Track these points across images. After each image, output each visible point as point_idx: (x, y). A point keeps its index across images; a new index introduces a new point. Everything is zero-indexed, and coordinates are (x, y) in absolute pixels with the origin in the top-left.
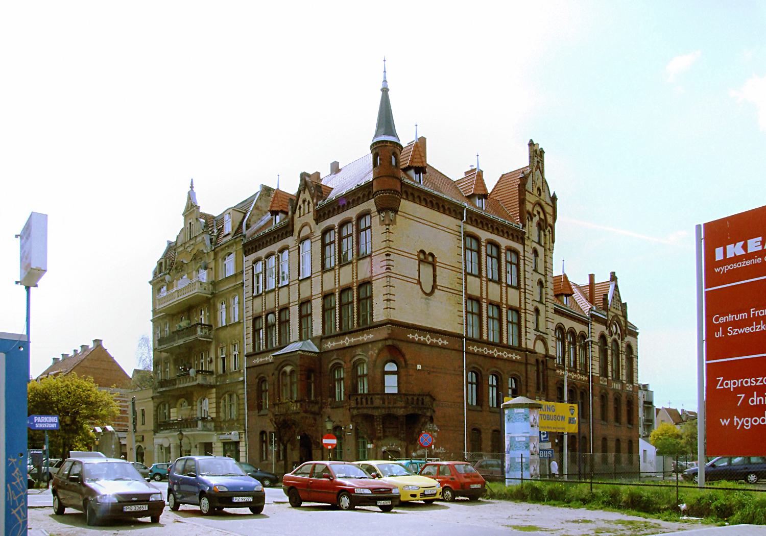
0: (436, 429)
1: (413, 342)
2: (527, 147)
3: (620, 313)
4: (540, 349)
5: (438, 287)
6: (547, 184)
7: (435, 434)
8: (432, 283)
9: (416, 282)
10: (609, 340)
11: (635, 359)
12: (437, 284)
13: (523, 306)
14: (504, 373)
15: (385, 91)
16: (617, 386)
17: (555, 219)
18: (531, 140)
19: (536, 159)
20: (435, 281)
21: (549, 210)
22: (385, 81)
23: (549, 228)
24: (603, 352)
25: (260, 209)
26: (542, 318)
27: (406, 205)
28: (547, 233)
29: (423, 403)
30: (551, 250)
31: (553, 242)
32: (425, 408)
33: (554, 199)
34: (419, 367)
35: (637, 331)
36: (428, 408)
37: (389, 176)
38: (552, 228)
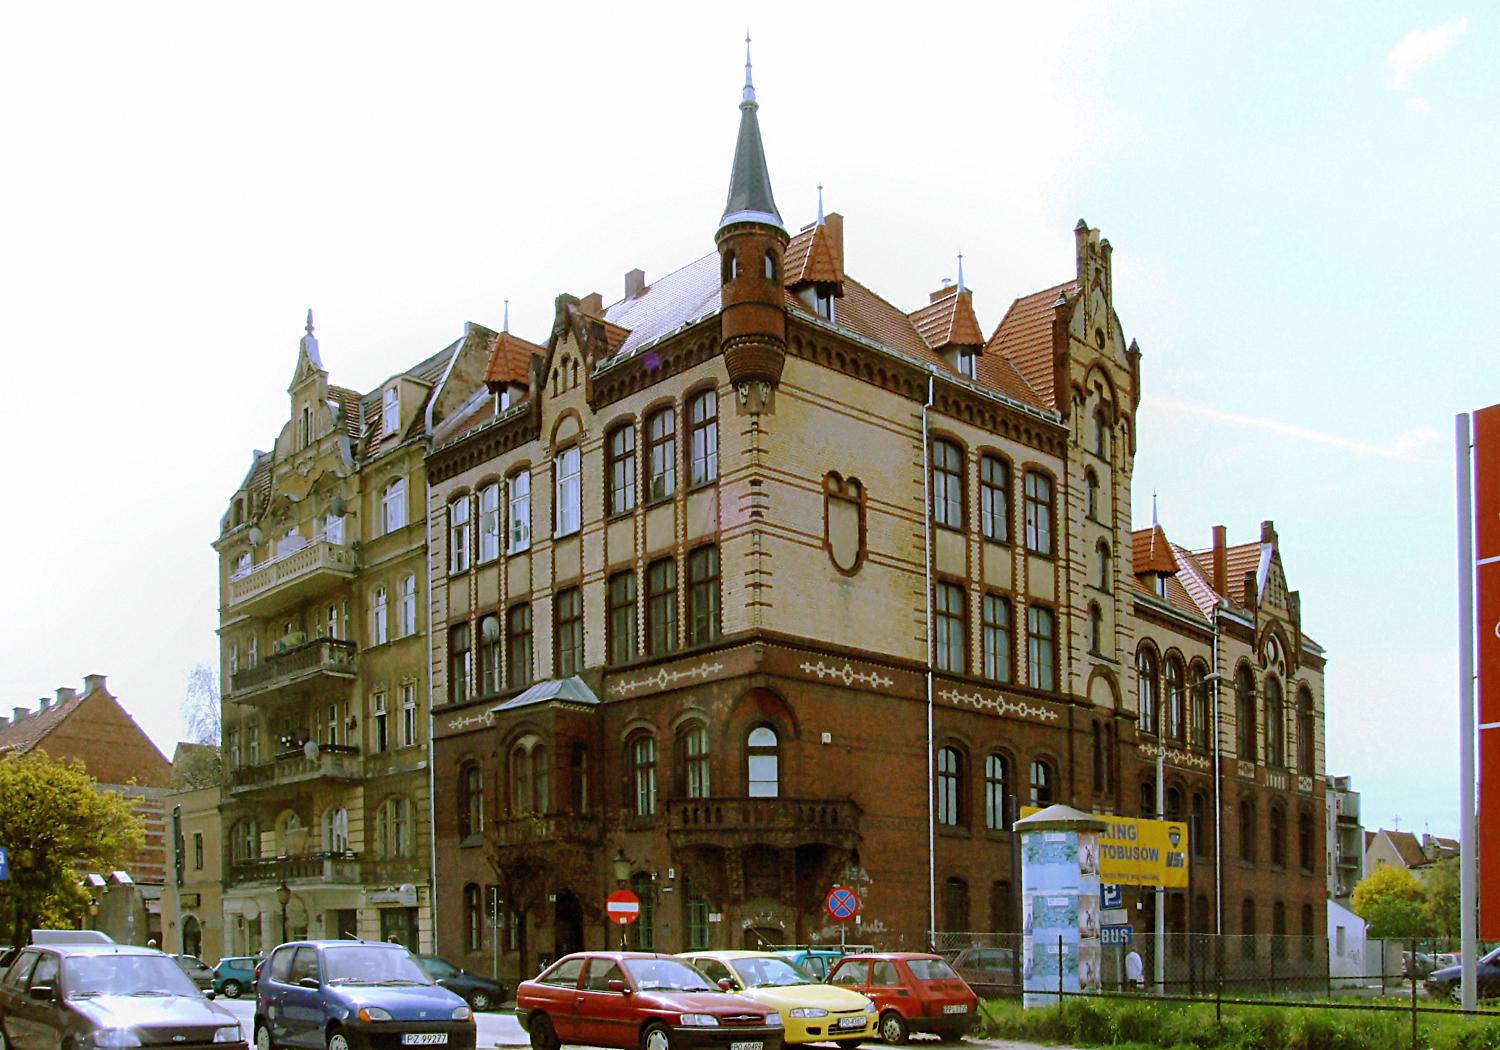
0: (866, 878)
1: (812, 680)
3: (1284, 615)
4: (1101, 696)
5: (871, 556)
6: (1117, 320)
7: (864, 890)
8: (855, 547)
9: (819, 543)
10: (1260, 676)
12: (868, 548)
13: (1063, 599)
15: (749, 109)
16: (1277, 781)
17: (1135, 401)
18: (1082, 222)
20: (862, 541)
21: (1122, 379)
22: (749, 87)
23: (1122, 421)
28: (1118, 433)
29: (835, 821)
30: (1127, 471)
31: (1132, 453)
32: (840, 832)
33: (1133, 355)
34: (827, 738)
35: (1323, 655)
36: (847, 832)
37: (758, 303)
38: (1130, 421)
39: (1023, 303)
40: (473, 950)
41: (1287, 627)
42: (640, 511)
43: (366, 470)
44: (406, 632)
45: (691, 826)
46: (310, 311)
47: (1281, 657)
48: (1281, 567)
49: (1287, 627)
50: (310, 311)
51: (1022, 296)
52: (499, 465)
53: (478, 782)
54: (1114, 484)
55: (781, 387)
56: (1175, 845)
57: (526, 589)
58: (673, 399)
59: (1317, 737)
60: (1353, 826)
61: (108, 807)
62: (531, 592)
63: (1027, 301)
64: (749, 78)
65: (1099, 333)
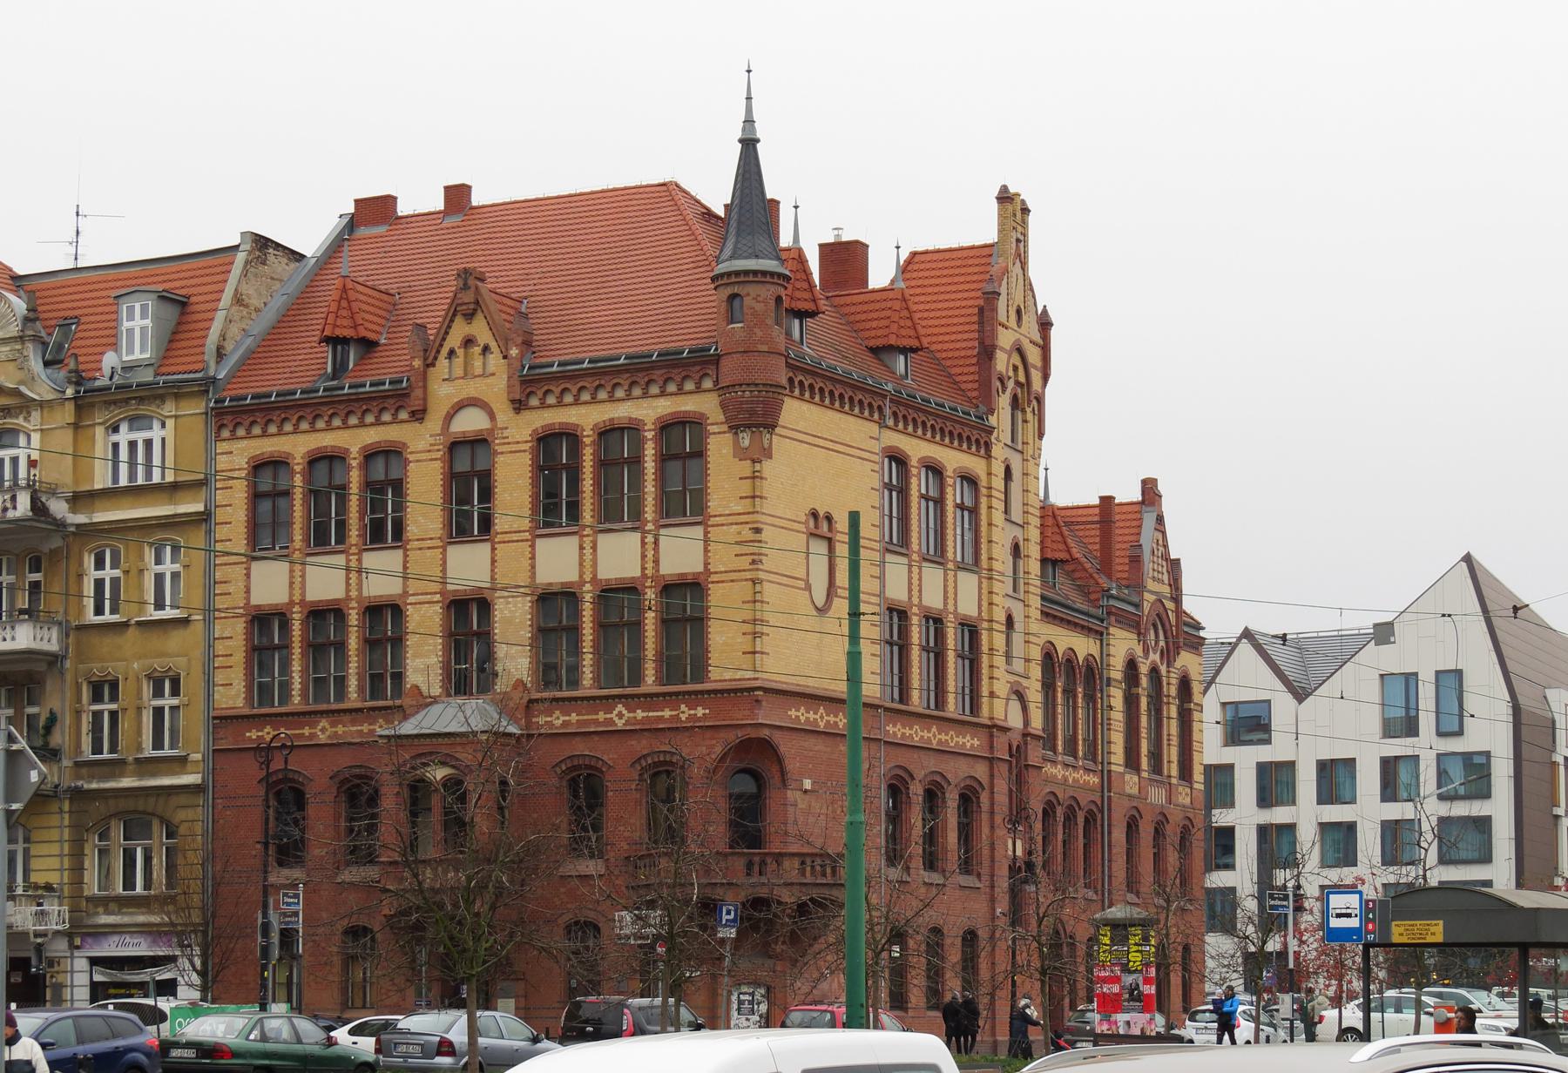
2: (994, 206)
3: (1166, 590)
4: (1015, 720)
6: (1032, 290)
9: (802, 584)
10: (1144, 669)
11: (1196, 715)
14: (913, 778)
15: (749, 145)
16: (1157, 796)
17: (1046, 377)
18: (1004, 189)
19: (1014, 235)
21: (1034, 355)
22: (749, 121)
23: (1035, 403)
24: (1131, 702)
25: (246, 301)
26: (1017, 638)
27: (796, 413)
28: (1029, 416)
30: (1036, 457)
31: (1041, 435)
33: (1045, 324)
35: (1202, 634)
38: (1040, 400)
39: (923, 258)
41: (1170, 605)
47: (1162, 643)
48: (1164, 533)
49: (1170, 605)
51: (920, 249)
53: (1204, 1011)
54: (1026, 474)
55: (777, 430)
58: (642, 422)
59: (1195, 736)
60: (649, 512)
63: (928, 257)
64: (749, 110)
65: (1019, 312)
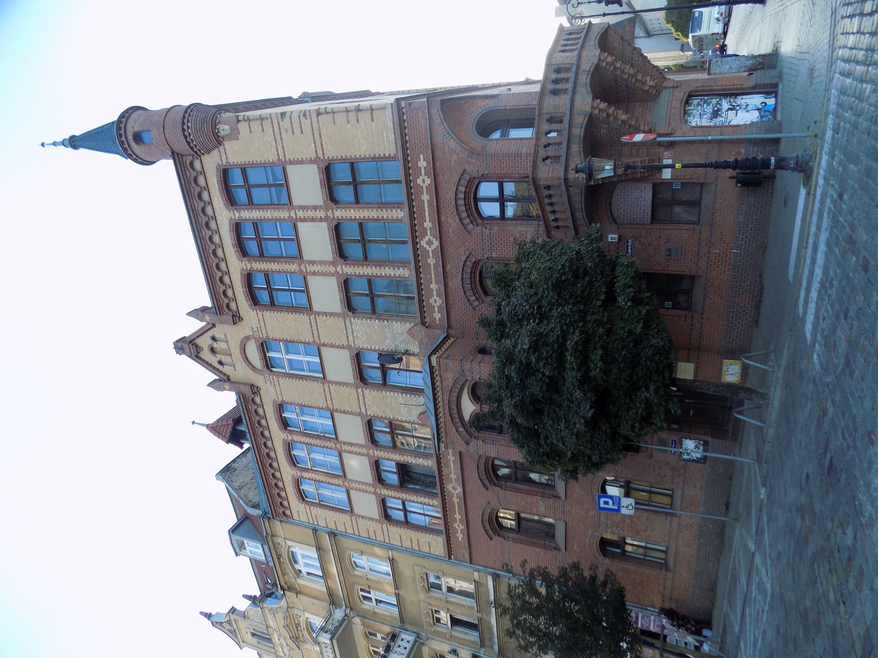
15: (74, 142)
40: (665, 560)
42: (338, 446)
43: (283, 583)
44: (388, 574)
45: (569, 86)
46: (201, 613)
50: (201, 613)
52: (287, 473)
56: (627, 507)
57: (373, 497)
61: (466, 610)
62: (349, 347)
